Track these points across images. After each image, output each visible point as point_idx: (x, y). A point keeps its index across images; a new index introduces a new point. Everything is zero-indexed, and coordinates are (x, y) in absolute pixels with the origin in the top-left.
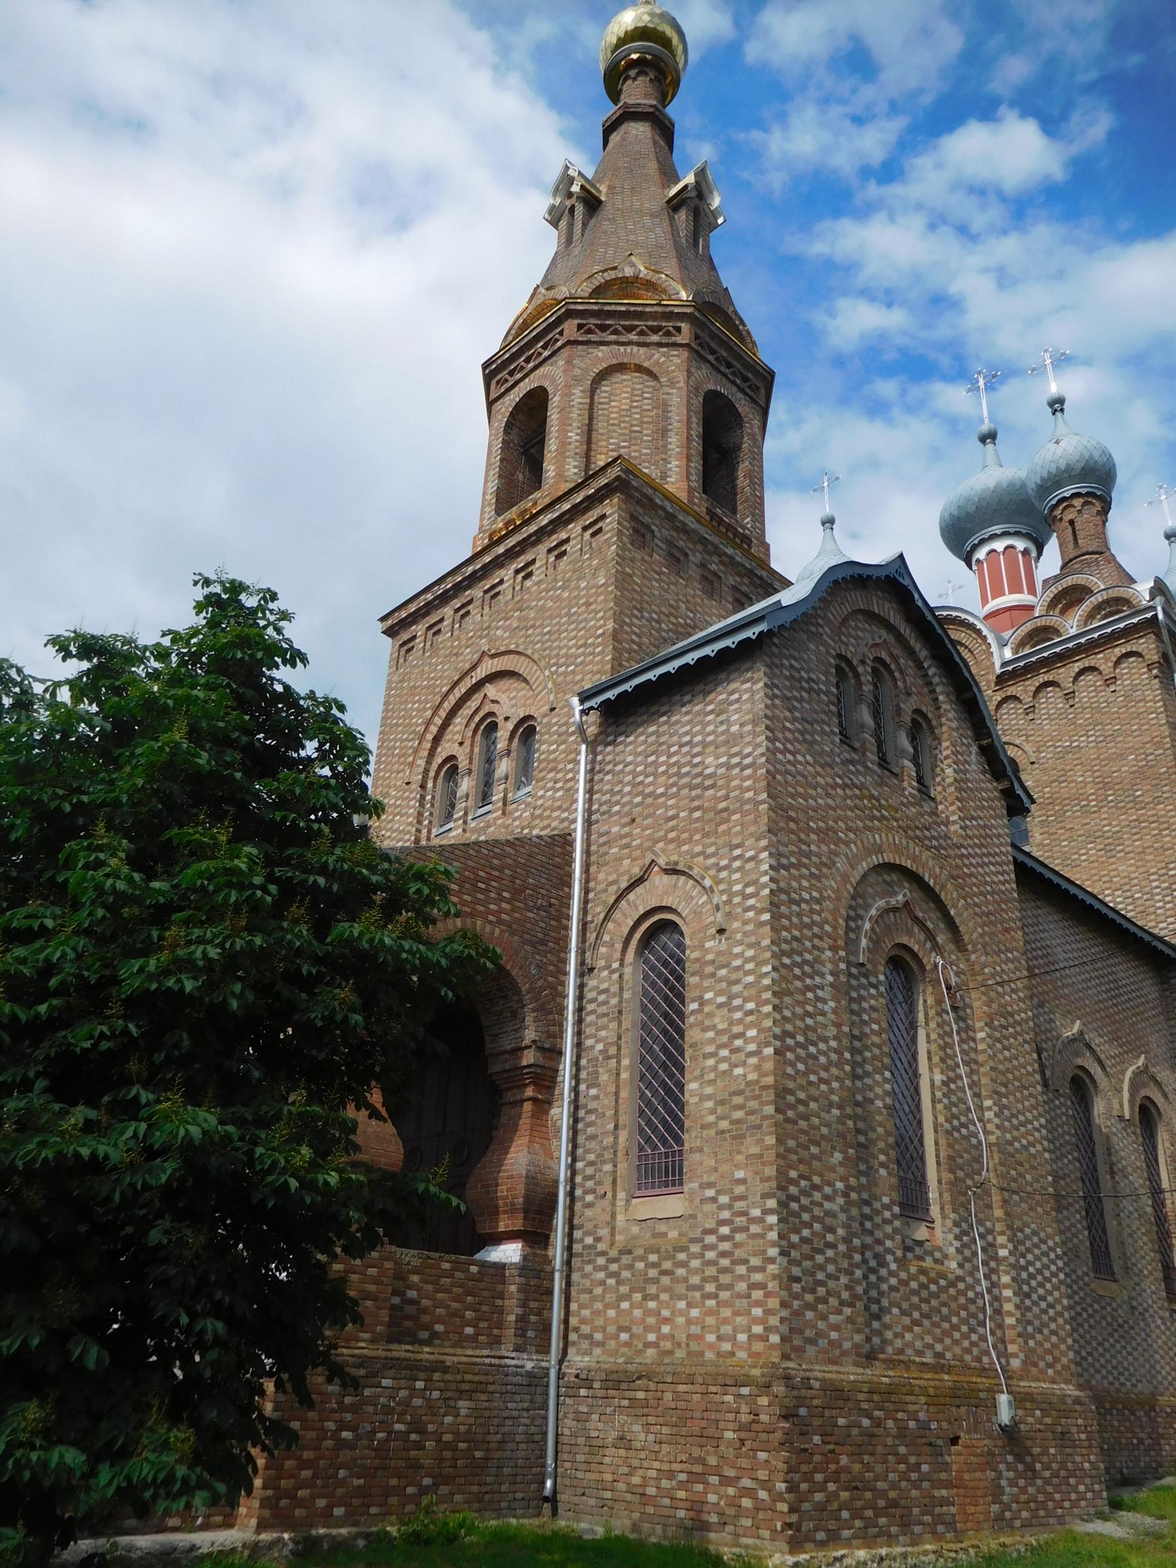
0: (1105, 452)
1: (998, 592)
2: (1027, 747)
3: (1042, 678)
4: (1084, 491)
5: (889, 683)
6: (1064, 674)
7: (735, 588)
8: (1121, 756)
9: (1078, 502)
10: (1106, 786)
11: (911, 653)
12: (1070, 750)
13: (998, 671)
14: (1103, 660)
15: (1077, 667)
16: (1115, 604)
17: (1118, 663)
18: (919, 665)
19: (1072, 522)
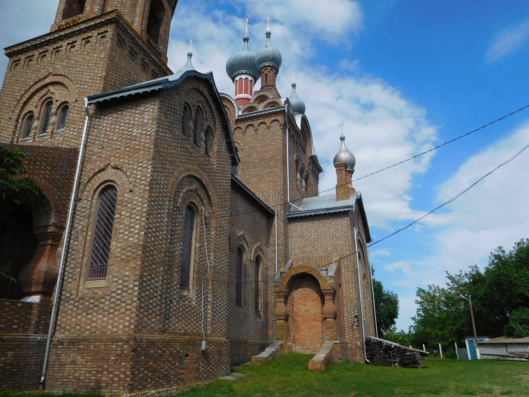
0: (280, 54)
1: (241, 92)
2: (241, 144)
3: (249, 123)
4: (271, 65)
5: (201, 115)
6: (256, 123)
7: (153, 71)
8: (268, 152)
9: (269, 68)
10: (262, 160)
11: (210, 106)
12: (254, 147)
13: (236, 118)
14: (267, 121)
15: (260, 121)
16: (274, 104)
17: (272, 122)
18: (212, 111)
19: (266, 75)
